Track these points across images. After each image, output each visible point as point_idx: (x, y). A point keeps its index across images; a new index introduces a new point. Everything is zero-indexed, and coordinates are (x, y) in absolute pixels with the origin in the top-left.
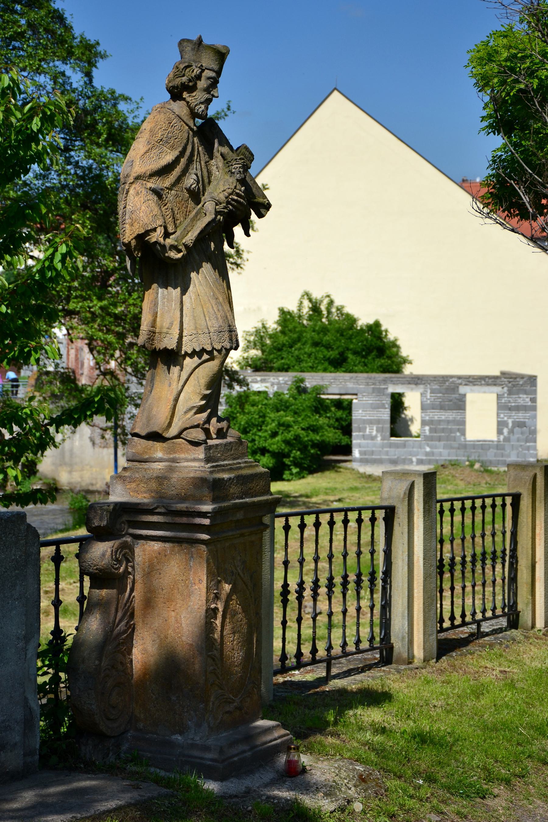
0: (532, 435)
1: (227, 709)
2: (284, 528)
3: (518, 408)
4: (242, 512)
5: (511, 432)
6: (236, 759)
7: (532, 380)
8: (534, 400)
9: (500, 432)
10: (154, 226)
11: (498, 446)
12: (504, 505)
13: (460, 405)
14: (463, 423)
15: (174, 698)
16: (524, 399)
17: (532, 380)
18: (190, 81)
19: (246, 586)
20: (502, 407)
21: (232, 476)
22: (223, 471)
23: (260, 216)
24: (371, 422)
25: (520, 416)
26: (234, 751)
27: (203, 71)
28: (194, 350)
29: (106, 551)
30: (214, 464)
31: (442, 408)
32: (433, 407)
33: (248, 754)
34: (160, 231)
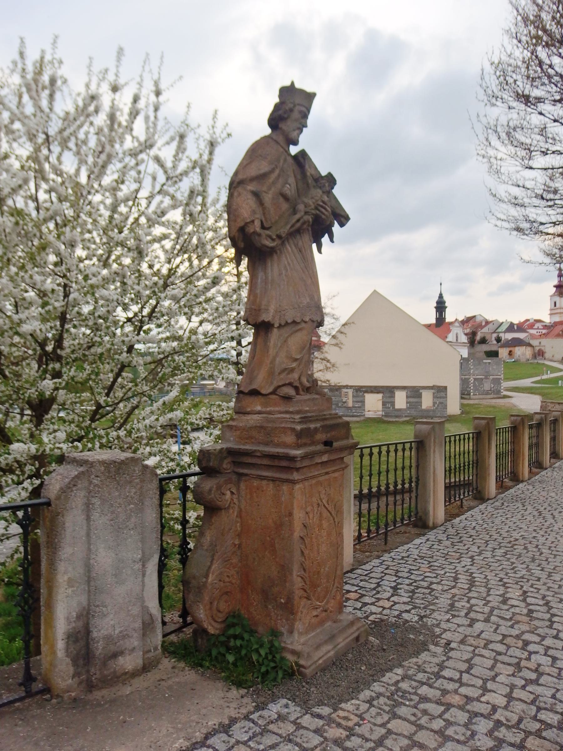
0: (445, 407)
1: (315, 613)
2: (360, 456)
3: (440, 397)
4: (326, 455)
5: (438, 406)
6: (320, 662)
7: (445, 388)
8: (446, 395)
9: (434, 406)
10: (252, 218)
11: (433, 411)
12: (469, 438)
13: (420, 396)
14: (421, 402)
15: (270, 607)
16: (442, 394)
17: (445, 388)
18: (285, 113)
19: (331, 514)
20: (434, 397)
21: (318, 425)
22: (311, 421)
23: (342, 225)
24: (388, 402)
25: (441, 400)
26: (320, 653)
27: (295, 106)
28: (287, 322)
29: (213, 487)
30: (303, 416)
31: (413, 397)
32: (410, 397)
33: (332, 653)
34: (257, 224)
